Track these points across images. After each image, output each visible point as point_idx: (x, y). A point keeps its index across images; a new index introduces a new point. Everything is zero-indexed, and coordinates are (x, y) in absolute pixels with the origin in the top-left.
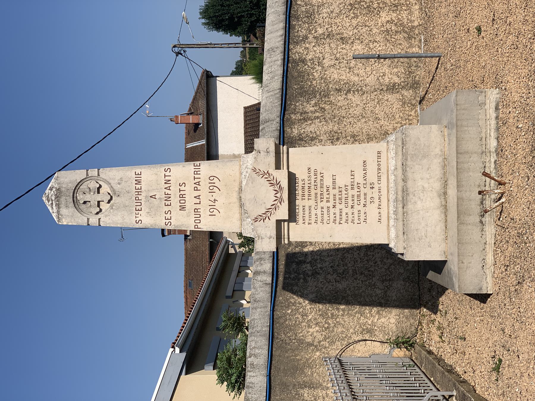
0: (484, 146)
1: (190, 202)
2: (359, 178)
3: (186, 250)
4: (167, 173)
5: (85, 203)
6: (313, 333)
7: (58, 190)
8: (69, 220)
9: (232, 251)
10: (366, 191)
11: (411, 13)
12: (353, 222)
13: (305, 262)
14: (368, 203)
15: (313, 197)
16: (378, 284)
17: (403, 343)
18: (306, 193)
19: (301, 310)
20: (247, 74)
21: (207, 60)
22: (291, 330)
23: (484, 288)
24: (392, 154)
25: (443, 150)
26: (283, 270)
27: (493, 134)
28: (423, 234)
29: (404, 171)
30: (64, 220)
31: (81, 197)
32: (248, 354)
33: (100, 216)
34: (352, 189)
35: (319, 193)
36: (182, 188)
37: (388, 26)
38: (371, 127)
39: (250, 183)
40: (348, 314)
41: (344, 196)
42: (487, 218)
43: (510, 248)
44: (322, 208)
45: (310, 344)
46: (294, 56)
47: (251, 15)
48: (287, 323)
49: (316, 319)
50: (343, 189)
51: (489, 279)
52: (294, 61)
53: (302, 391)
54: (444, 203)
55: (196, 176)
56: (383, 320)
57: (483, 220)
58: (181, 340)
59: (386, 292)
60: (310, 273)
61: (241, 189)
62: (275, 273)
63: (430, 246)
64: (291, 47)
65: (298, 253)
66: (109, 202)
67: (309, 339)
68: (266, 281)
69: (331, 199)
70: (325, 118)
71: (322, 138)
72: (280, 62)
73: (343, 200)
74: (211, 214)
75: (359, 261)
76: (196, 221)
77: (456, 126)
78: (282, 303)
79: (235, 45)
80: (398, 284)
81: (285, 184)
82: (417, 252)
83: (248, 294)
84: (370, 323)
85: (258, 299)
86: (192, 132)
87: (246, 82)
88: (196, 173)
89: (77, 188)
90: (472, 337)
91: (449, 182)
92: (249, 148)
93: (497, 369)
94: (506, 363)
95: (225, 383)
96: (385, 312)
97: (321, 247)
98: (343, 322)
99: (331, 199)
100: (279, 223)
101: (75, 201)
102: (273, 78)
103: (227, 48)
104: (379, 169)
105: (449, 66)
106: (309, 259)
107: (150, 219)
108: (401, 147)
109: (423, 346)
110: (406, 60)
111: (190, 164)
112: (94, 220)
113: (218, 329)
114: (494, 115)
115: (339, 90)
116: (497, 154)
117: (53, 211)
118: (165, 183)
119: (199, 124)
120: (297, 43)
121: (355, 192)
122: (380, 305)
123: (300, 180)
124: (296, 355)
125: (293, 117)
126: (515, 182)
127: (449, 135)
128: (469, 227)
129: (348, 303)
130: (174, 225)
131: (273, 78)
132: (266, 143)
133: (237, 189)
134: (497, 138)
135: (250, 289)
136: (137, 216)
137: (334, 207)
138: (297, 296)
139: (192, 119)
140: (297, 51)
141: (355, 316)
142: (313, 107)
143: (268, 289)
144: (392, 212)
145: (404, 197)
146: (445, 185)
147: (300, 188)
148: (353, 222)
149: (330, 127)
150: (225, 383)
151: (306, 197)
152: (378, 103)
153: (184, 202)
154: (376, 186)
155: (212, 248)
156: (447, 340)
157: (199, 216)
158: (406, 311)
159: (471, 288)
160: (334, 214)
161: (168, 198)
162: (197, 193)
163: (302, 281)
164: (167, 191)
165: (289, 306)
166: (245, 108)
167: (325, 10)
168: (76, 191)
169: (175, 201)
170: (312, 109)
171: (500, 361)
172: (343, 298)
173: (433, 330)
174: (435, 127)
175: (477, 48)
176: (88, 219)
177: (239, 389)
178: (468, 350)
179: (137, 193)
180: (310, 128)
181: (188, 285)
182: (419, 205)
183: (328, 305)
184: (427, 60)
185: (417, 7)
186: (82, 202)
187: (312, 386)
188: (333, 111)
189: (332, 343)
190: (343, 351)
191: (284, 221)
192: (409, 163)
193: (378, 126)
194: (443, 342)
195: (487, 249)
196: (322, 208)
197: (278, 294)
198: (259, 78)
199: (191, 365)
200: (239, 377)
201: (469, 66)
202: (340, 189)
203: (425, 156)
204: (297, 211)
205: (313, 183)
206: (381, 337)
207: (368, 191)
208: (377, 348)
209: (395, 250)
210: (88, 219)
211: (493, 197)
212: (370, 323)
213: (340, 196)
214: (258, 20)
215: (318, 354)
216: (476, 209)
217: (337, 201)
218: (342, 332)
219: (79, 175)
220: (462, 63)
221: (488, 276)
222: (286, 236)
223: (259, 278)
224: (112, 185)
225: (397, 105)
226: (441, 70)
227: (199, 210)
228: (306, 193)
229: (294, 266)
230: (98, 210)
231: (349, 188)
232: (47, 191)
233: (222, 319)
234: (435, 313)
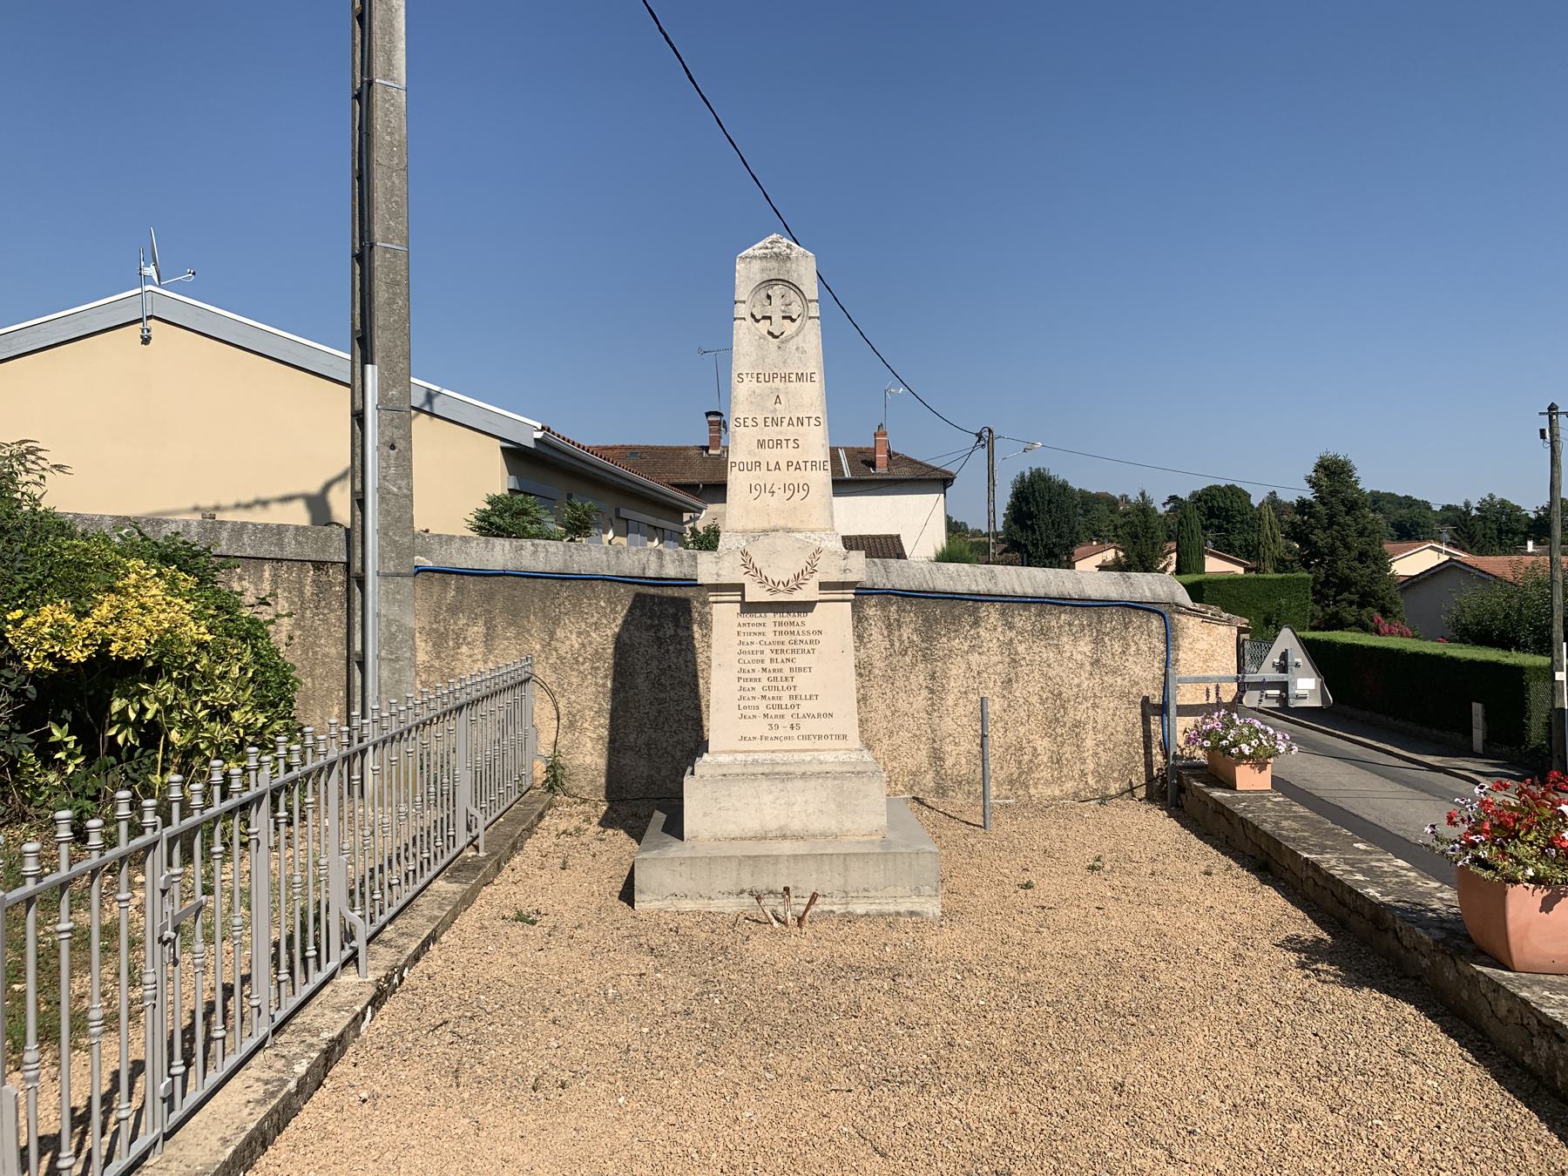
2: (806, 707)
3: (686, 448)
4: (813, 421)
5: (769, 297)
6: (570, 639)
7: (788, 257)
8: (743, 273)
9: (686, 517)
10: (788, 717)
11: (1048, 783)
13: (677, 626)
14: (770, 721)
15: (779, 638)
17: (554, 776)
18: (784, 628)
20: (948, 538)
21: (971, 480)
22: (574, 606)
23: (643, 897)
24: (843, 757)
27: (874, 908)
29: (818, 775)
31: (777, 291)
32: (537, 541)
33: (750, 319)
36: (791, 444)
37: (1028, 750)
38: (879, 725)
41: (780, 684)
42: (748, 900)
43: (703, 935)
45: (552, 635)
46: (984, 609)
47: (1035, 545)
50: (790, 683)
51: (656, 905)
52: (977, 609)
53: (481, 622)
56: (589, 745)
57: (746, 895)
58: (553, 440)
60: (660, 634)
61: (790, 531)
62: (660, 582)
63: (705, 814)
64: (998, 605)
66: (770, 333)
67: (560, 633)
72: (974, 588)
77: (885, 853)
79: (992, 521)
81: (798, 596)
82: (695, 794)
83: (623, 541)
87: (937, 538)
90: (566, 879)
91: (801, 843)
92: (851, 543)
93: (520, 917)
94: (531, 931)
95: (489, 507)
96: (602, 748)
100: (740, 588)
101: (770, 282)
102: (952, 578)
103: (987, 510)
104: (820, 737)
105: (972, 840)
107: (744, 397)
109: (550, 805)
110: (979, 776)
113: (570, 496)
114: (902, 909)
115: (933, 677)
116: (844, 915)
117: (755, 250)
119: (874, 467)
120: (1003, 614)
121: (786, 701)
122: (612, 741)
124: (535, 614)
125: (893, 608)
126: (803, 942)
127: (872, 842)
128: (735, 873)
129: (615, 691)
131: (952, 578)
132: (858, 567)
134: (867, 915)
135: (630, 544)
137: (764, 670)
139: (881, 457)
140: (991, 614)
143: (637, 572)
145: (778, 775)
146: (798, 837)
147: (761, 620)
149: (879, 664)
150: (489, 507)
151: (778, 629)
154: (795, 733)
155: (689, 488)
156: (561, 841)
161: (777, 422)
162: (783, 465)
164: (786, 421)
167: (1051, 655)
169: (772, 432)
170: (905, 637)
171: (533, 923)
173: (574, 821)
174: (883, 821)
175: (1001, 883)
177: (480, 528)
178: (546, 874)
180: (876, 632)
181: (633, 452)
182: (767, 798)
184: (980, 809)
185: (1057, 793)
187: (489, 638)
189: (555, 669)
190: (543, 685)
191: (743, 596)
192: (830, 783)
193: (880, 736)
194: (558, 836)
195: (701, 901)
198: (945, 557)
199: (516, 455)
200: (498, 528)
201: (973, 872)
203: (839, 805)
206: (563, 742)
207: (788, 721)
208: (547, 736)
209: (699, 762)
211: (780, 909)
214: (1029, 555)
215: (538, 647)
216: (761, 886)
217: (772, 675)
218: (570, 684)
219: (811, 288)
220: (977, 860)
223: (653, 558)
225: (911, 764)
226: (965, 829)
228: (784, 628)
231: (792, 692)
232: (785, 241)
233: (586, 503)
234: (600, 824)
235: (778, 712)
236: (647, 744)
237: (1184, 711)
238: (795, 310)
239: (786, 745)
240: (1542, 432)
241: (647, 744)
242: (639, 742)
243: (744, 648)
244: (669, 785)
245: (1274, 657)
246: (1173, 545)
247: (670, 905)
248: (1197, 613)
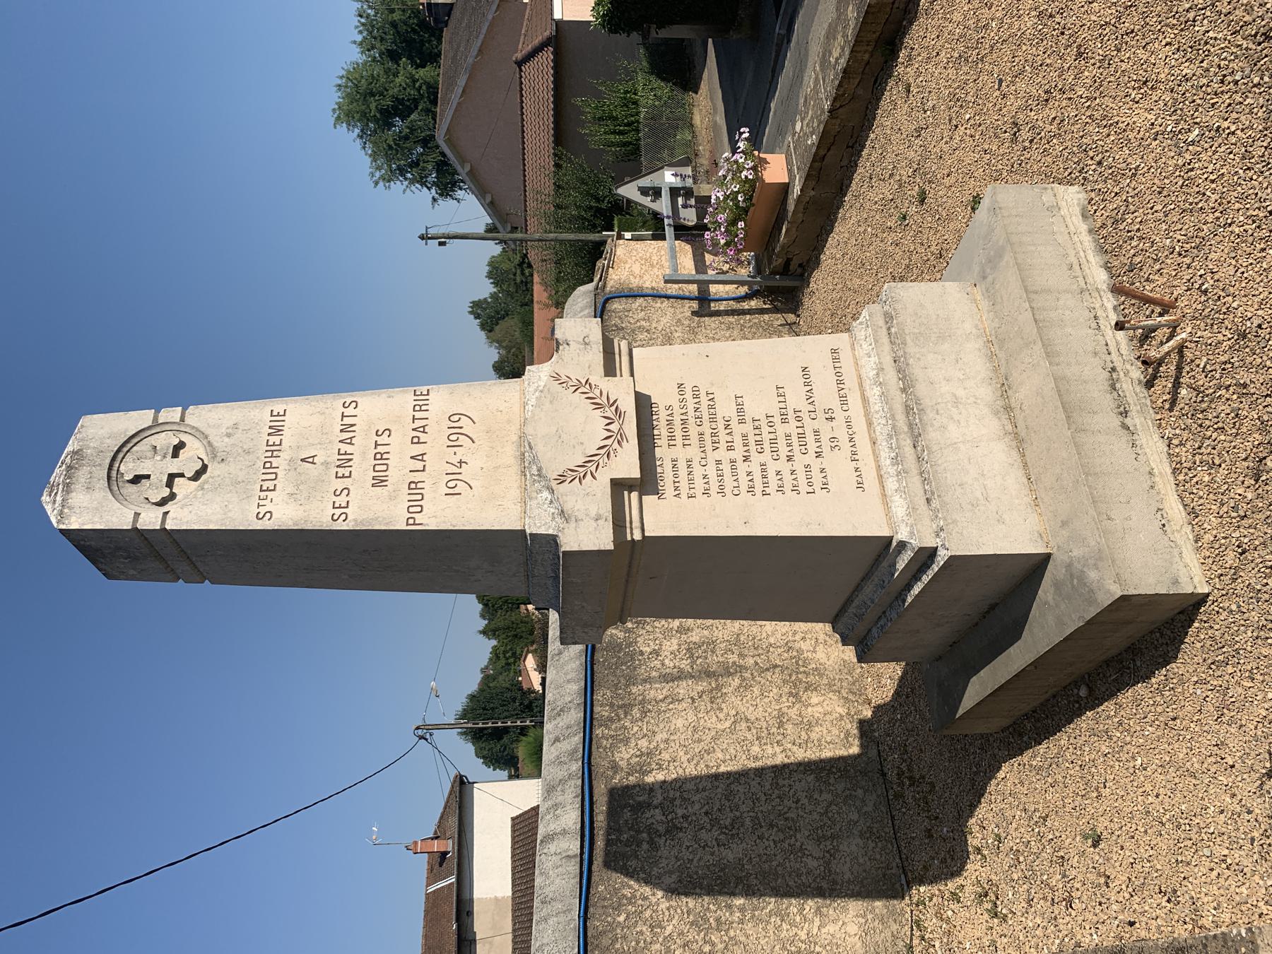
0: (1080, 279)
1: (399, 468)
2: (796, 399)
4: (348, 412)
5: (137, 480)
10: (816, 425)
12: (795, 489)
13: (649, 805)
15: (694, 439)
16: (809, 848)
18: (678, 434)
19: (648, 913)
23: (1184, 579)
25: (981, 326)
26: (604, 825)
28: (978, 494)
30: (73, 519)
34: (784, 421)
35: (708, 432)
39: (547, 405)
40: (752, 917)
41: (766, 437)
44: (718, 462)
48: (618, 946)
49: (682, 934)
50: (764, 423)
54: (1009, 428)
55: (418, 415)
56: (831, 928)
59: (828, 863)
60: (661, 829)
63: (1000, 521)
65: (634, 786)
68: (568, 850)
73: (767, 446)
74: (451, 491)
75: (763, 798)
76: (411, 509)
78: (605, 899)
80: (851, 846)
84: (804, 937)
85: (551, 895)
86: (437, 866)
88: (417, 408)
89: (125, 449)
97: (681, 772)
98: (743, 939)
100: (619, 487)
104: (840, 382)
106: (658, 799)
108: (884, 330)
111: (406, 392)
112: (152, 515)
118: (342, 431)
122: (820, 893)
123: (662, 408)
129: (749, 892)
130: (355, 520)
133: (515, 438)
136: (262, 503)
137: (746, 459)
138: (638, 880)
139: (436, 846)
141: (768, 922)
143: (573, 867)
144: (888, 462)
145: (913, 422)
147: (668, 466)
148: (795, 489)
151: (679, 441)
153: (384, 468)
154: (839, 415)
157: (419, 497)
158: (878, 904)
159: (1151, 580)
160: (749, 474)
161: (345, 460)
162: (417, 449)
163: (645, 846)
164: (344, 448)
165: (620, 905)
166: (513, 819)
168: (121, 455)
169: (362, 468)
172: (739, 880)
176: (137, 515)
179: (269, 454)
182: (954, 432)
183: (706, 899)
186: (129, 477)
192: (911, 349)
196: (718, 462)
197: (595, 878)
202: (757, 423)
203: (942, 338)
204: (659, 470)
207: (821, 423)
210: (137, 515)
212: (804, 937)
213: (758, 438)
217: (753, 447)
221: (1184, 549)
222: (636, 523)
224: (210, 438)
227: (419, 485)
228: (678, 434)
229: (627, 814)
230: (166, 492)
231: (777, 419)
235: (810, 438)
236: (819, 841)
237: (700, 266)
238: (166, 440)
239: (860, 425)
240: (441, 244)
241: (819, 841)
242: (817, 853)
243: (714, 488)
244: (869, 808)
245: (646, 201)
246: (523, 607)
247: (1183, 536)
248: (605, 271)
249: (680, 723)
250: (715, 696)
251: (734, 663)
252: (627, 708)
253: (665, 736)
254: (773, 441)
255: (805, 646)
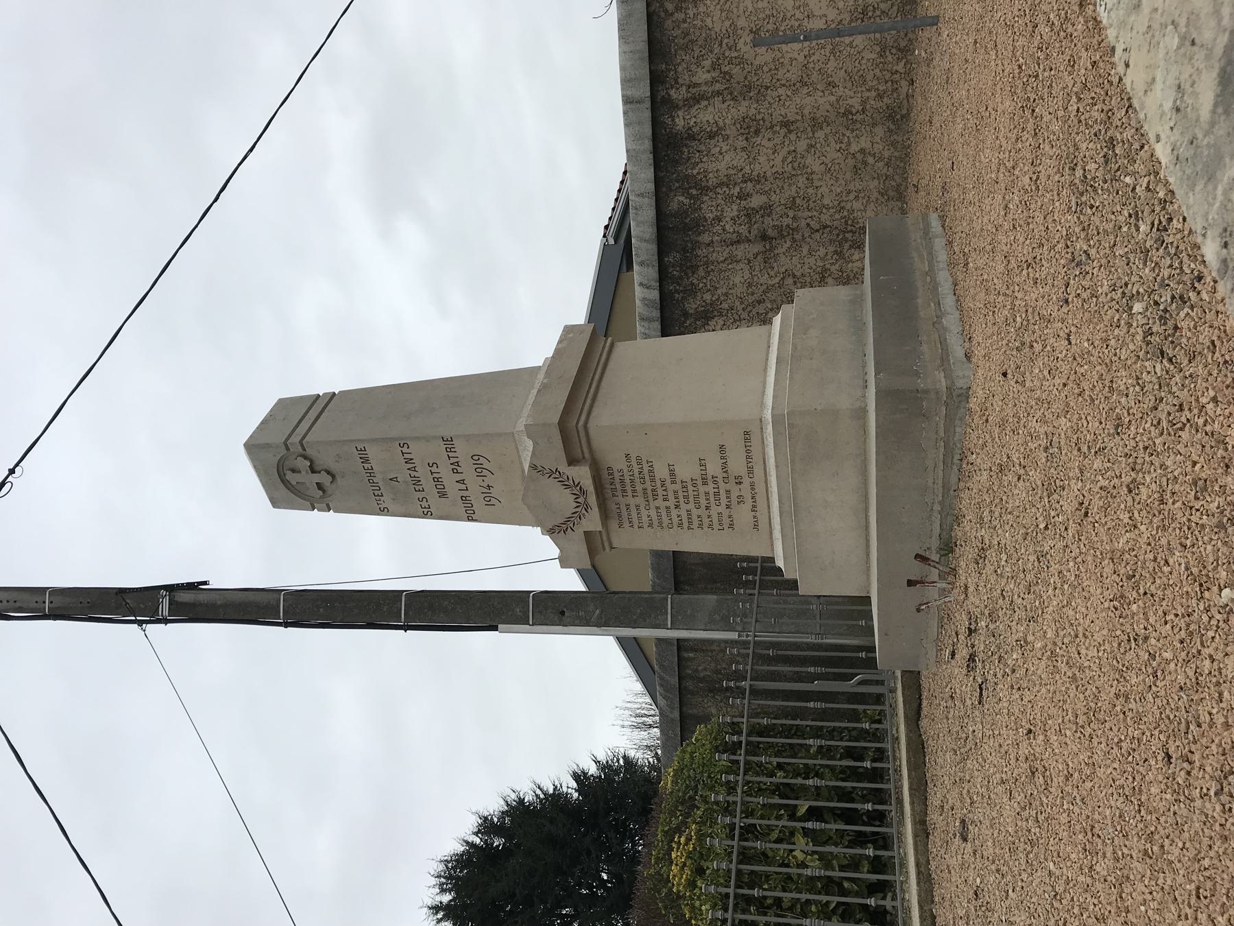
2: (714, 468)
10: (728, 487)
12: (710, 526)
15: (640, 493)
35: (650, 488)
36: (434, 469)
44: (657, 508)
69: (671, 496)
70: (731, 94)
71: (728, 132)
73: (691, 499)
81: (588, 483)
99: (671, 496)
121: (710, 488)
142: (709, 72)
149: (743, 109)
151: (630, 493)
152: (832, 52)
154: (746, 481)
161: (417, 482)
162: (459, 477)
170: (708, 76)
188: (746, 78)
196: (657, 508)
205: (637, 475)
207: (732, 486)
228: (629, 488)
231: (700, 482)
243: (656, 523)
249: (737, 280)
250: (768, 259)
251: (788, 226)
252: (694, 269)
253: (724, 290)
254: (696, 497)
255: (857, 205)
